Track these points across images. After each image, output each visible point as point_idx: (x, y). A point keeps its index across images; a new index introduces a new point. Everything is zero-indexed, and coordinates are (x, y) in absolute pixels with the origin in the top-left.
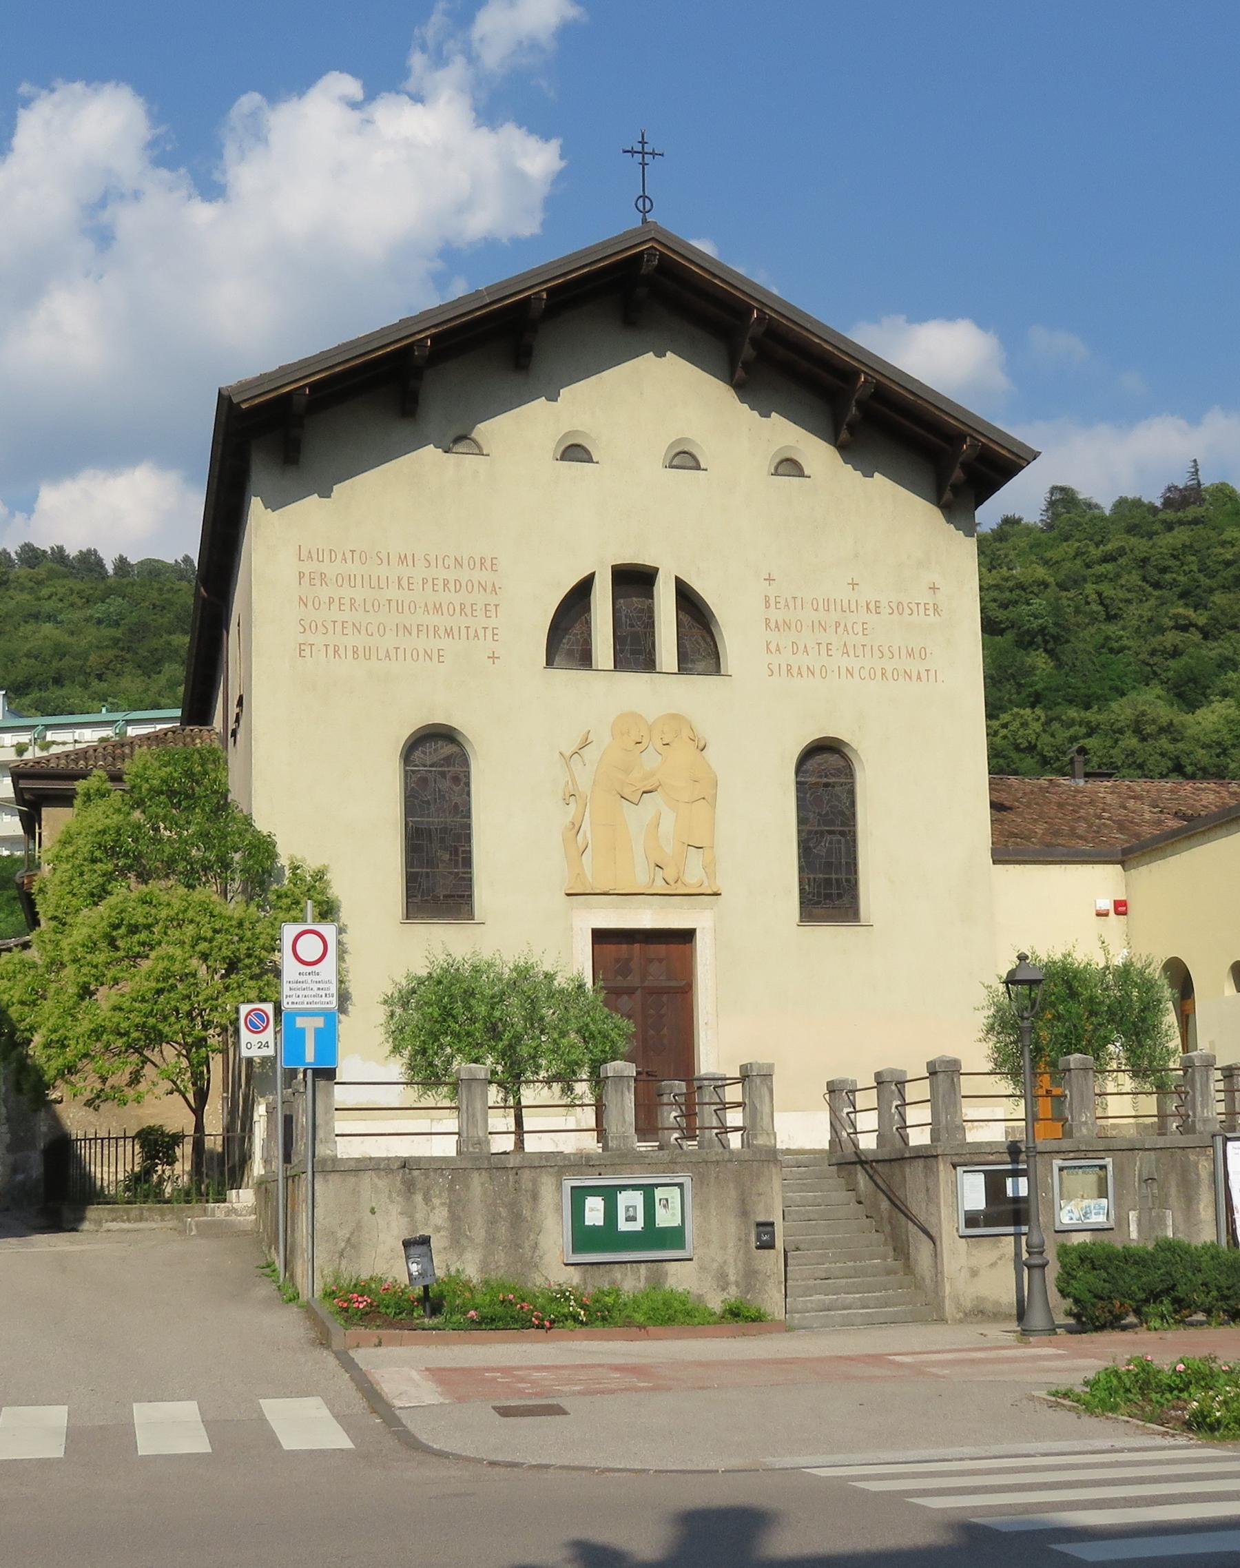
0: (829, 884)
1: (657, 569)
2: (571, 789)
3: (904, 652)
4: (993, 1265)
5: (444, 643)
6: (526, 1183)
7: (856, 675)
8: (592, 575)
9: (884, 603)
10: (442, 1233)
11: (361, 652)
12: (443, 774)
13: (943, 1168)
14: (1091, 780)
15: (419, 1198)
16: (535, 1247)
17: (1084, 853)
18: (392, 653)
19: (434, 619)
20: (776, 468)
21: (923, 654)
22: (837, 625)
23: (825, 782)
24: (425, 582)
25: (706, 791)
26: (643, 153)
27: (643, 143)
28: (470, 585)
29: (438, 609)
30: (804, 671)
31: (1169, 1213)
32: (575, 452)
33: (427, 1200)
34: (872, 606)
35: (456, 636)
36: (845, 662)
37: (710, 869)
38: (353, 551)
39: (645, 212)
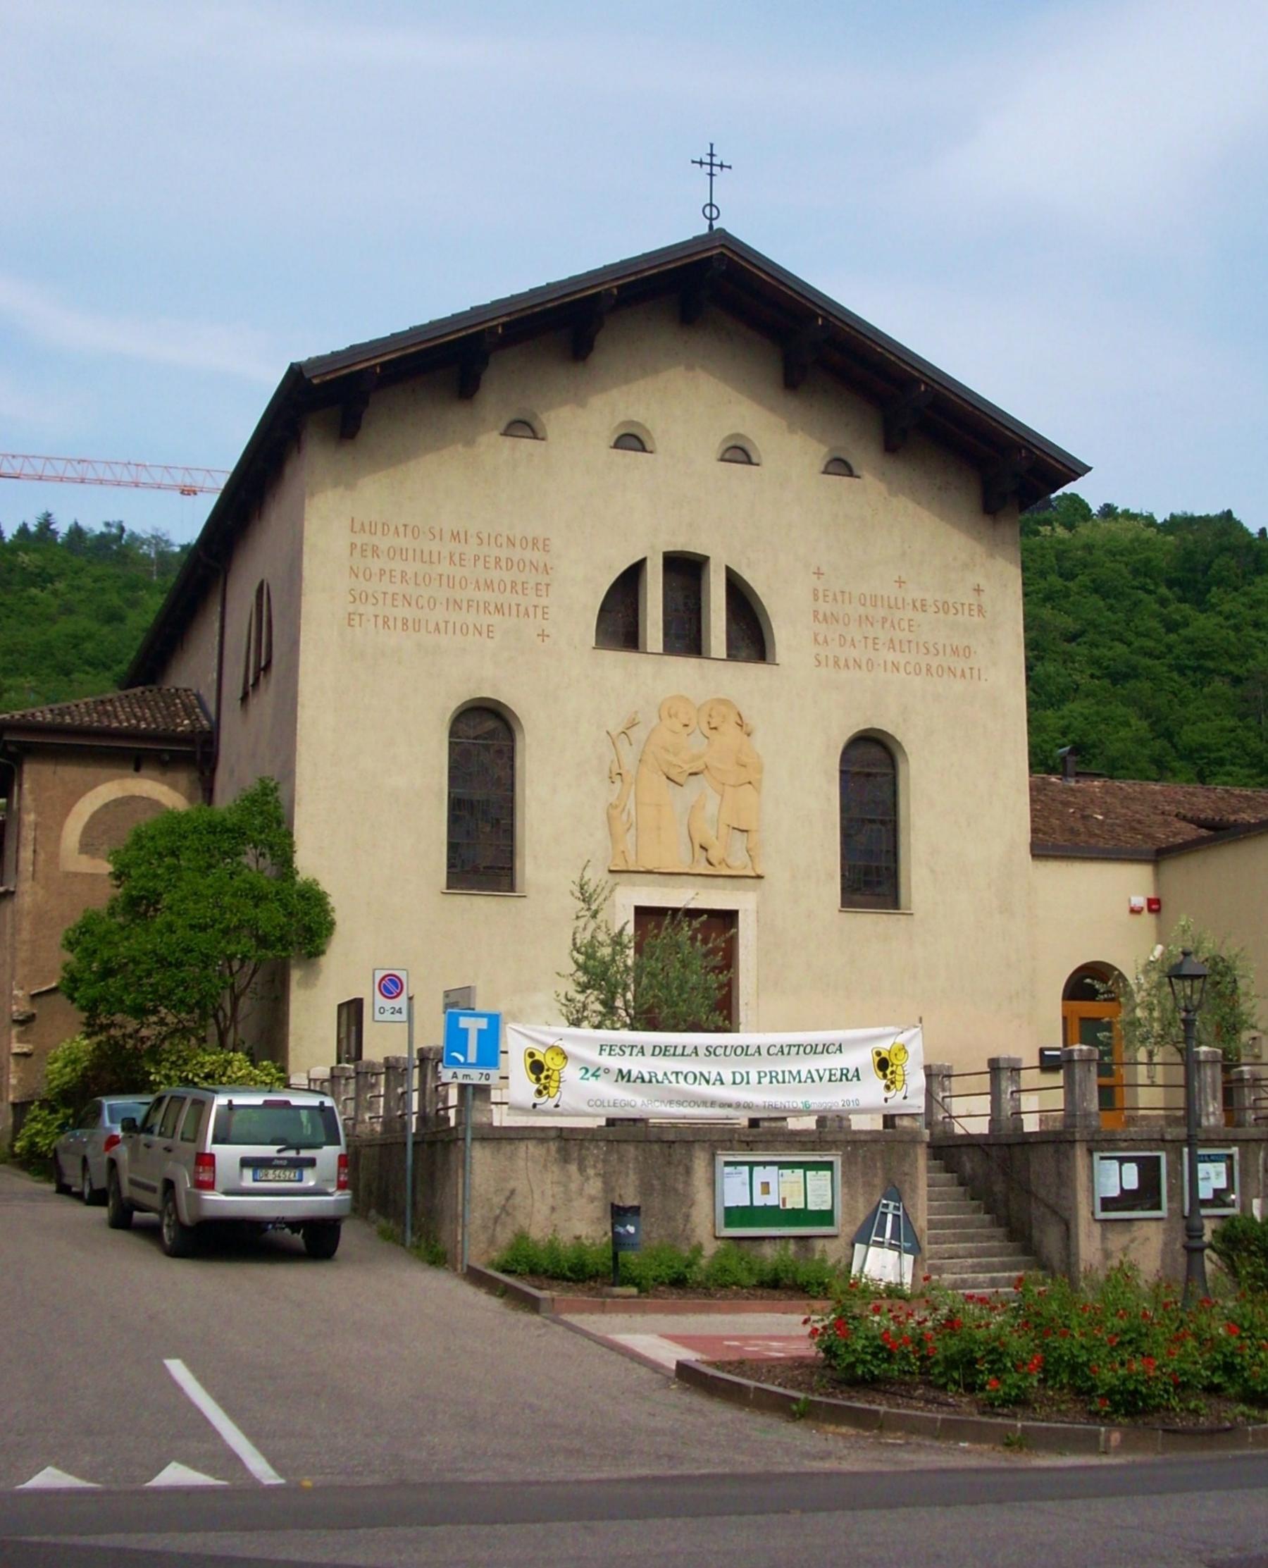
0: (872, 874)
1: (707, 559)
2: (616, 770)
3: (948, 650)
5: (496, 619)
7: (902, 670)
8: (643, 561)
9: (930, 602)
10: (596, 1204)
11: (410, 624)
12: (487, 747)
13: (1080, 1151)
14: (1082, 780)
15: (573, 1168)
16: (687, 1217)
17: (1056, 847)
18: (442, 626)
19: (484, 595)
20: (826, 467)
21: (968, 652)
22: (884, 620)
23: (871, 769)
24: (476, 558)
25: (748, 775)
26: (712, 164)
27: (712, 155)
28: (521, 565)
29: (489, 585)
30: (851, 663)
32: (631, 440)
33: (582, 1169)
34: (918, 604)
35: (506, 611)
36: (891, 656)
38: (405, 526)
39: (711, 219)
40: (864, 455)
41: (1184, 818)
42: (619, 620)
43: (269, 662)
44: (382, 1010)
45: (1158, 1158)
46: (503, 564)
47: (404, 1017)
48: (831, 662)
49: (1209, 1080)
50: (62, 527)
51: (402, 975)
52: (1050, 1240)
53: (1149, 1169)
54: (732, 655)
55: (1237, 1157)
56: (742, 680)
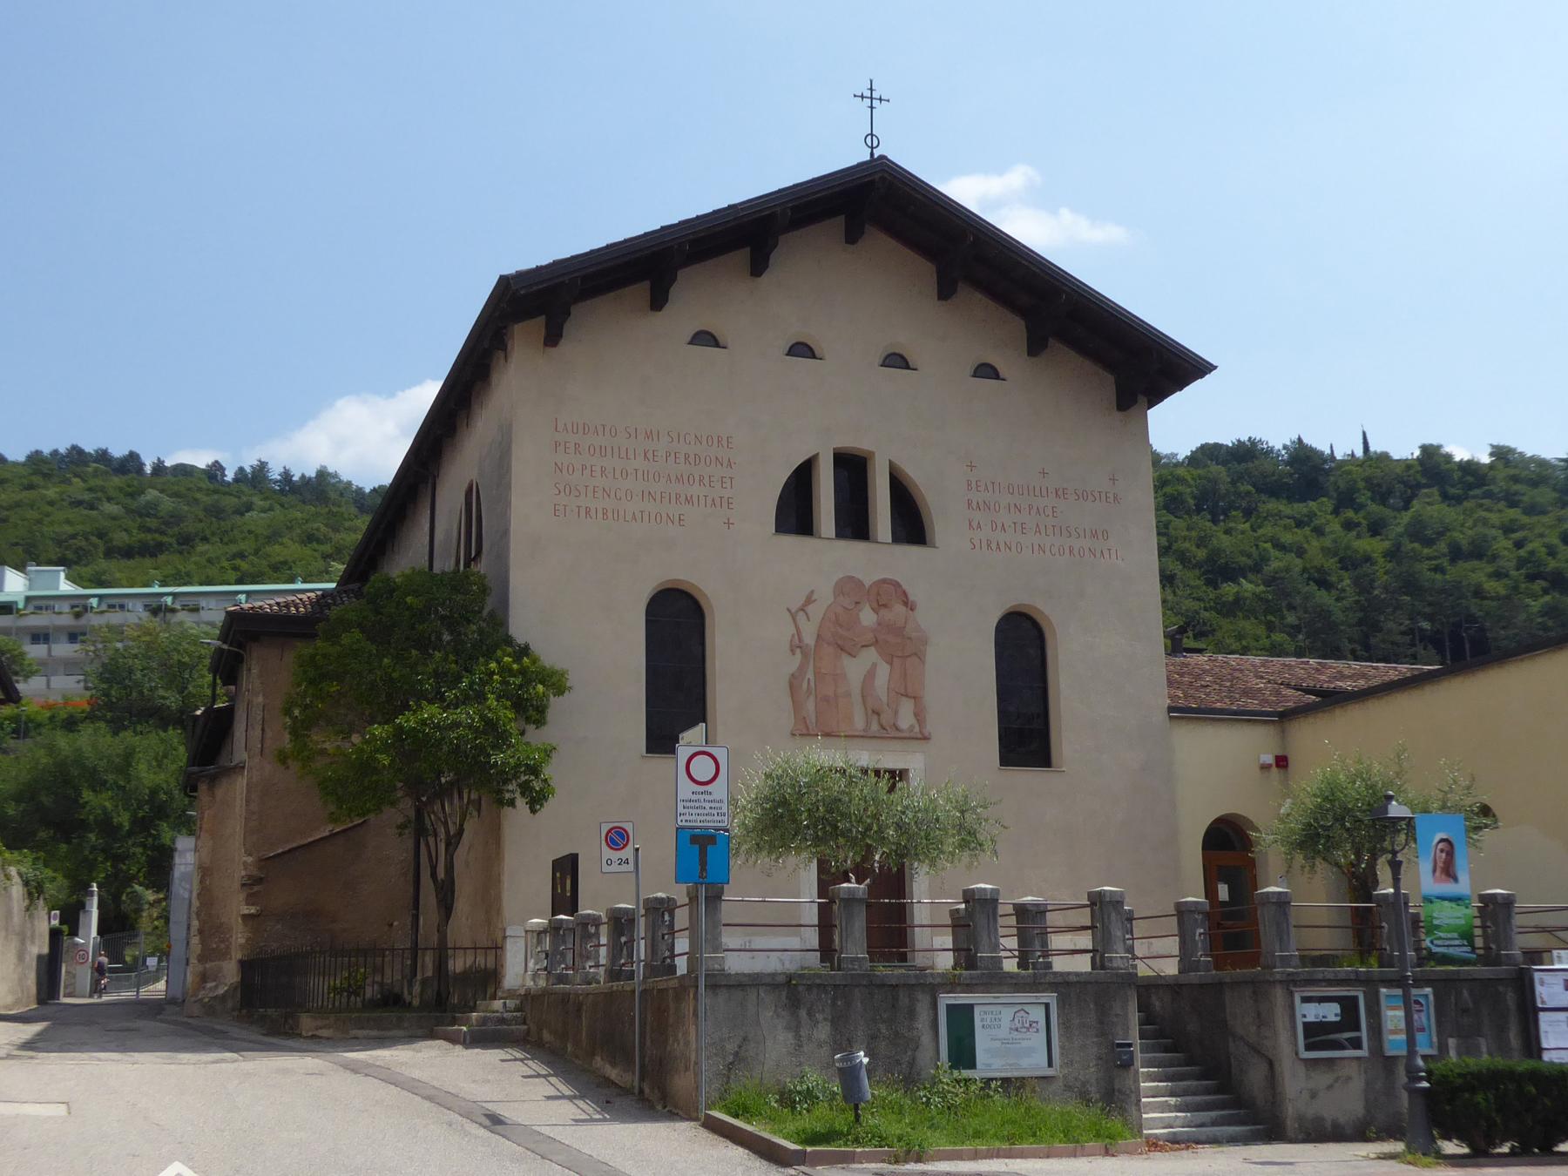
4: (1330, 1087)
6: (904, 1000)
8: (815, 457)
13: (1279, 994)
15: (803, 1013)
18: (639, 516)
23: (1022, 646)
31: (1482, 1041)
37: (919, 715)
40: (1011, 361)
41: (1288, 686)
42: (795, 513)
43: (479, 552)
44: (609, 862)
45: (1356, 998)
46: (691, 459)
47: (631, 867)
48: (984, 545)
49: (218, 1027)
50: (275, 473)
51: (629, 827)
52: (1255, 1077)
53: (1348, 1005)
54: (897, 539)
55: (1431, 998)
56: (902, 562)
